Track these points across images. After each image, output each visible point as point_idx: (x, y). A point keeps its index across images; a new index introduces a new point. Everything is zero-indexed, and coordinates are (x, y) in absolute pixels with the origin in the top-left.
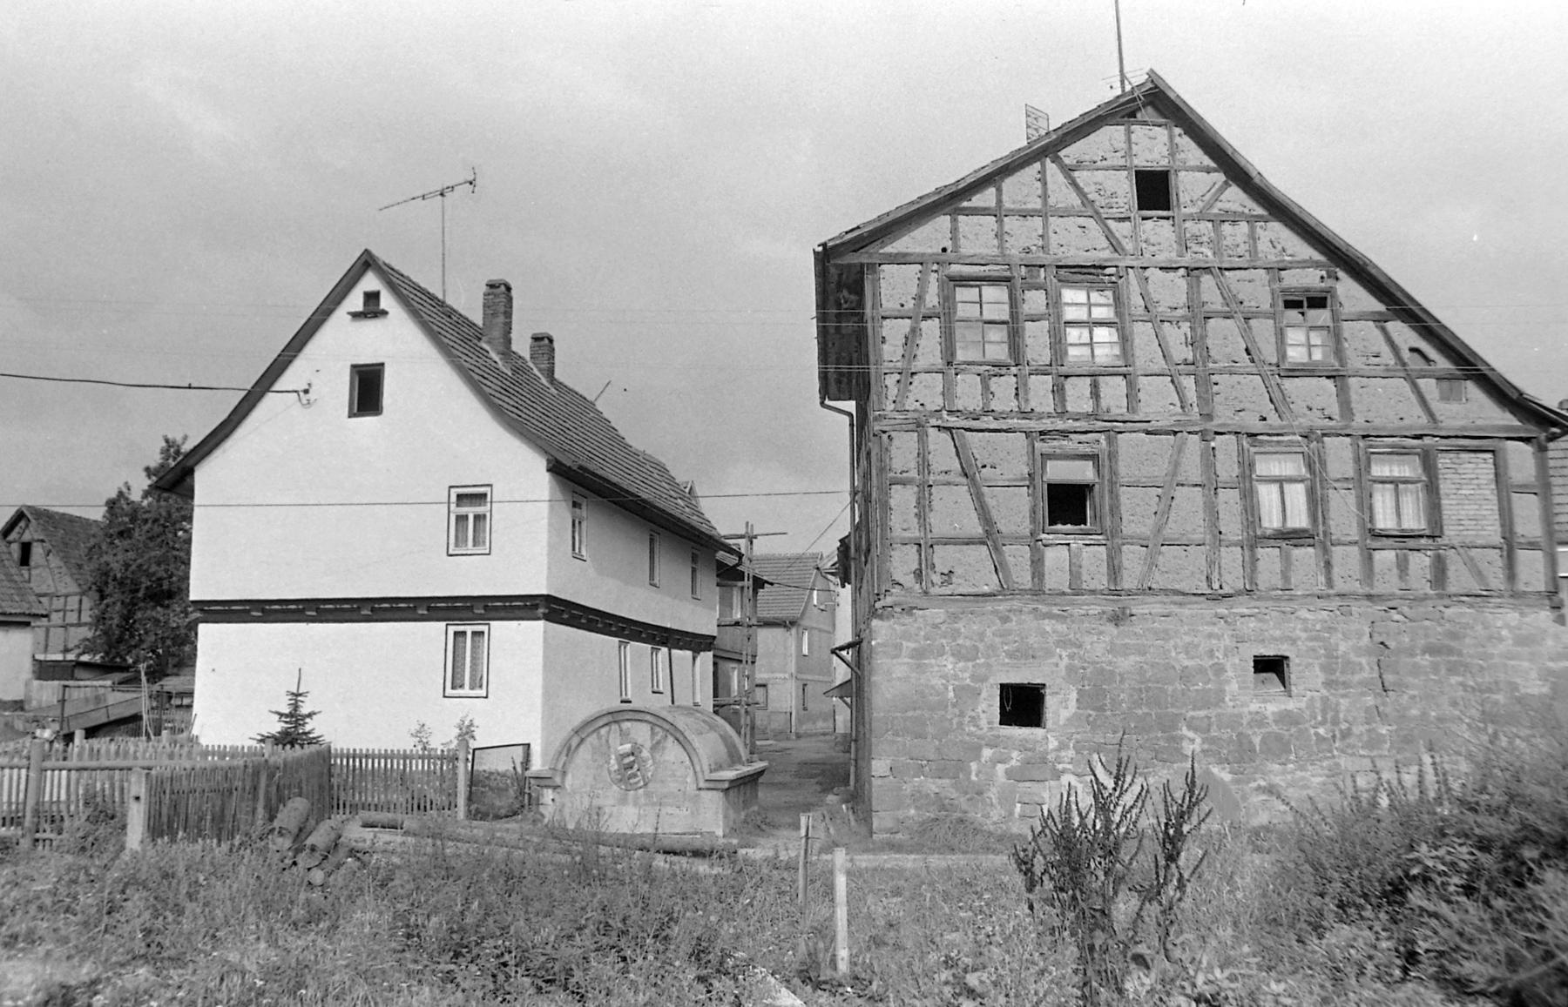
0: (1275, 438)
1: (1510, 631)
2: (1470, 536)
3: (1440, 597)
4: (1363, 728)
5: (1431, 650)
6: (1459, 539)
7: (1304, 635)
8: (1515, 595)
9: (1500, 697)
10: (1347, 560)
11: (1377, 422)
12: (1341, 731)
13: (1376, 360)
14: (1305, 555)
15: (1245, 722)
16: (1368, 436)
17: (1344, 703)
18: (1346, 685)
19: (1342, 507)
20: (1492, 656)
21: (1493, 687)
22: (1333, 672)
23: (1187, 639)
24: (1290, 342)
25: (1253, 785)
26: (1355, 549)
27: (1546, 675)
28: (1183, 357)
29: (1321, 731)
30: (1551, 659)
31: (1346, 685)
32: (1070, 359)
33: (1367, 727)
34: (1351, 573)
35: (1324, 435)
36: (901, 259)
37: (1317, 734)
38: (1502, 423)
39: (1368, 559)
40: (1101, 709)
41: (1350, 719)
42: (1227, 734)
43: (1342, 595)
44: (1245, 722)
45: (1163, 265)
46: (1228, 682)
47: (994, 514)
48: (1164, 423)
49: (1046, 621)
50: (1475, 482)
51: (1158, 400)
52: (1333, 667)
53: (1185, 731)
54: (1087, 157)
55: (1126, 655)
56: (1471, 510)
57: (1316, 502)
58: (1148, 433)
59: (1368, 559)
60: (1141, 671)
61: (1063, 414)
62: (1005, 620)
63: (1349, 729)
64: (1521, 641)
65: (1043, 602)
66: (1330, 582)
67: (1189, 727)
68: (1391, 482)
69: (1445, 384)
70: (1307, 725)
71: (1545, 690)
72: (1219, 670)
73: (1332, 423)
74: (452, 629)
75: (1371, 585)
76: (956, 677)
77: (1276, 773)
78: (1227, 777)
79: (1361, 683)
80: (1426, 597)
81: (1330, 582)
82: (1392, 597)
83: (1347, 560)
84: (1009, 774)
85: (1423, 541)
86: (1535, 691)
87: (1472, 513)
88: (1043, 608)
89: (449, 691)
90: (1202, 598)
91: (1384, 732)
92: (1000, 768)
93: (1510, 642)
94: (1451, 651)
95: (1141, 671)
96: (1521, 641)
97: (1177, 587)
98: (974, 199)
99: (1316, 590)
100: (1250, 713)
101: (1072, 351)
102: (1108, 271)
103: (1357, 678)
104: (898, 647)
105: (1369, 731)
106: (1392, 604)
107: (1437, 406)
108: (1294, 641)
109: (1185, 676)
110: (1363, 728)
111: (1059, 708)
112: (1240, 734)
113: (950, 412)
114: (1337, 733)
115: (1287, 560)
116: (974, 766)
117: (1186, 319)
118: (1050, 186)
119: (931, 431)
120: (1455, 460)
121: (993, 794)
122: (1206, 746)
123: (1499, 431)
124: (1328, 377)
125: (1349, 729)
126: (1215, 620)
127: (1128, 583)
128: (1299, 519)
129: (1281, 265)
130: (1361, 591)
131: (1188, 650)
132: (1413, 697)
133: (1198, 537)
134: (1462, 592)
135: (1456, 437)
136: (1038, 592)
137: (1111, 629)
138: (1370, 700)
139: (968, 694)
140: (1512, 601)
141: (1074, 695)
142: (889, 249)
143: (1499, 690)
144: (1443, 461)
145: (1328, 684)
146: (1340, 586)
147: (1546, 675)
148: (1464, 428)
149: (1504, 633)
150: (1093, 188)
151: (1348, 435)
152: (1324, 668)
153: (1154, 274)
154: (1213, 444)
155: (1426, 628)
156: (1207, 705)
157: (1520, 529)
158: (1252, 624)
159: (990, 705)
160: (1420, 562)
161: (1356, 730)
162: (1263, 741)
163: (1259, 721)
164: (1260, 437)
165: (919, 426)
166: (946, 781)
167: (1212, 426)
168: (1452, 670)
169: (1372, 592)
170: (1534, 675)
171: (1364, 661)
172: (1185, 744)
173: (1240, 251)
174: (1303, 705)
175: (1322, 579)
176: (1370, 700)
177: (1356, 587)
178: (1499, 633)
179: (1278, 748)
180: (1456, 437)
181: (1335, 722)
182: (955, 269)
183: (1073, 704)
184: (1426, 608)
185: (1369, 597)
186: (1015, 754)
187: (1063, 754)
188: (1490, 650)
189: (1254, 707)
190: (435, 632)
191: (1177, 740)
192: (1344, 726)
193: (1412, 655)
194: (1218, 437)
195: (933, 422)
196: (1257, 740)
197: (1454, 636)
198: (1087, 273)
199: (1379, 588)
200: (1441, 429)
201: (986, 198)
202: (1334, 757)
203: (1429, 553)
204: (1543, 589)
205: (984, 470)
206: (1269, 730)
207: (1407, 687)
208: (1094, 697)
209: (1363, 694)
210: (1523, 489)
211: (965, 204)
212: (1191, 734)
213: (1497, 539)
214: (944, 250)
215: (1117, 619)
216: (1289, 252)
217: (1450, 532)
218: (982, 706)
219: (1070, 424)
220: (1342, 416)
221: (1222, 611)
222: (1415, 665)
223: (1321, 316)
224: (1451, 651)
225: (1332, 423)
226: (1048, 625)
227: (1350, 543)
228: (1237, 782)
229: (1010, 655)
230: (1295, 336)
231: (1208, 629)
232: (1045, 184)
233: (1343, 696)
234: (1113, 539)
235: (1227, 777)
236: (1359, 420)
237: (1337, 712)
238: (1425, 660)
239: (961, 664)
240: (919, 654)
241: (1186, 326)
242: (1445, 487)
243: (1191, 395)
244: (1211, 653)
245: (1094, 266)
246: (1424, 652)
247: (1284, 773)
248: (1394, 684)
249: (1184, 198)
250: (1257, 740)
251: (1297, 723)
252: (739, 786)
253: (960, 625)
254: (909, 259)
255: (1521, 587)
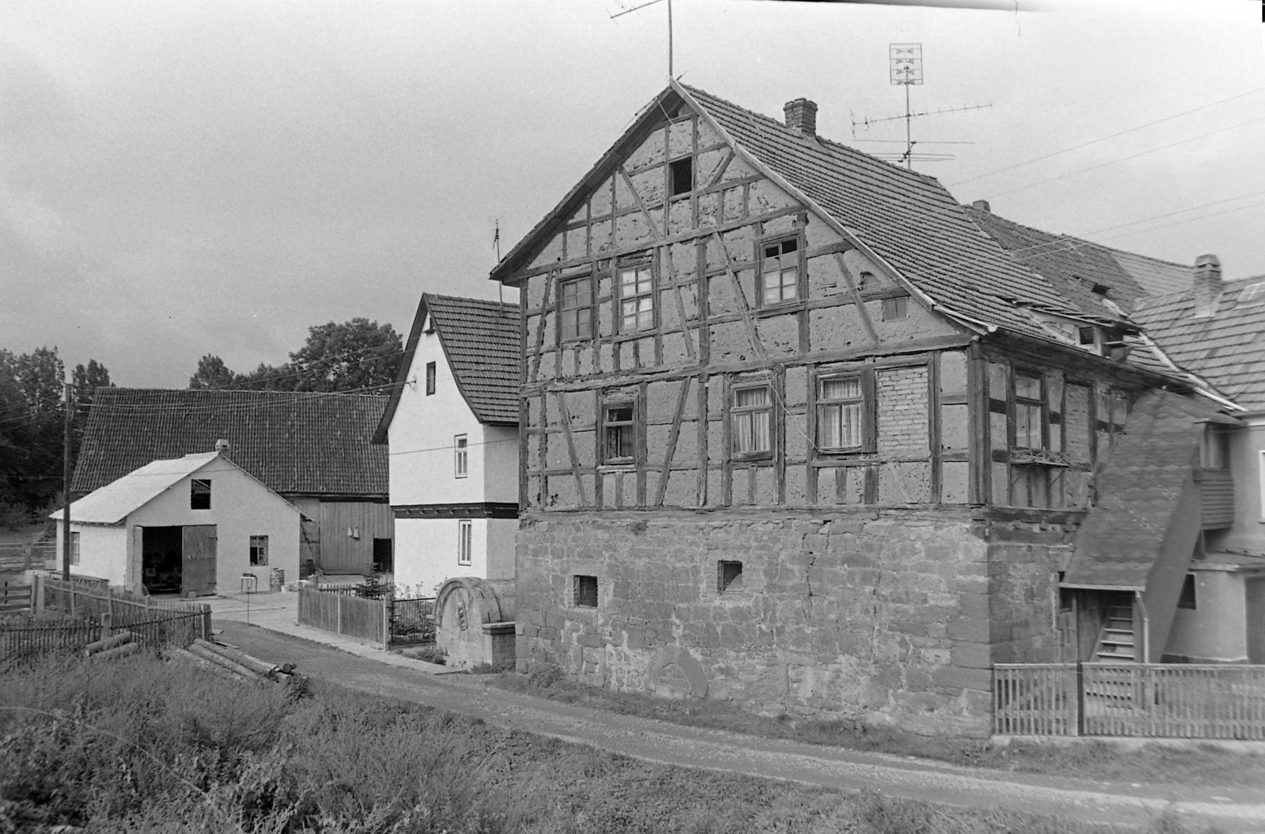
0: (751, 374)
1: (924, 544)
2: (903, 451)
3: (869, 510)
4: (794, 627)
5: (849, 560)
6: (892, 454)
7: (755, 544)
8: (940, 507)
9: (911, 609)
10: (797, 476)
11: (830, 349)
12: (777, 628)
13: (833, 291)
14: (766, 475)
15: (711, 614)
16: (820, 363)
17: (780, 605)
18: (782, 589)
19: (797, 428)
20: (905, 568)
21: (904, 597)
22: (773, 577)
23: (677, 546)
24: (768, 286)
25: (717, 666)
26: (804, 467)
27: (955, 588)
28: (692, 313)
29: (763, 627)
30: (961, 573)
31: (782, 589)
32: (625, 328)
33: (796, 626)
34: (799, 490)
35: (787, 367)
36: (537, 272)
37: (760, 629)
38: (938, 335)
39: (814, 473)
40: (626, 597)
41: (784, 619)
42: (701, 623)
43: (791, 510)
44: (711, 614)
45: (682, 239)
46: (701, 581)
47: (577, 455)
48: (676, 371)
49: (601, 531)
50: (909, 397)
51: (677, 353)
52: (774, 572)
53: (674, 619)
54: (640, 163)
55: (639, 557)
56: (904, 425)
57: (778, 429)
58: (669, 380)
59: (814, 473)
60: (649, 570)
61: (618, 372)
62: (578, 529)
63: (782, 627)
64: (933, 553)
65: (600, 516)
66: (782, 499)
67: (678, 617)
68: (837, 404)
69: (891, 304)
70: (754, 621)
71: (953, 603)
72: (696, 571)
73: (791, 355)
74: (462, 523)
75: (815, 501)
76: (553, 570)
77: (731, 658)
78: (699, 657)
79: (792, 587)
80: (857, 511)
81: (782, 499)
82: (830, 510)
83: (797, 476)
84: (579, 640)
85: (861, 458)
86: (944, 604)
87: (905, 428)
88: (600, 520)
89: (462, 562)
90: (694, 513)
91: (809, 632)
92: (575, 635)
93: (923, 554)
94: (866, 562)
95: (649, 570)
96: (933, 553)
97: (679, 504)
98: (576, 216)
99: (771, 506)
100: (715, 608)
101: (792, 281)
102: (649, 252)
103: (790, 583)
104: (526, 547)
105: (798, 630)
106: (827, 517)
107: (878, 326)
108: (747, 549)
109: (674, 574)
110: (794, 627)
111: (606, 593)
112: (708, 624)
113: (559, 380)
114: (774, 630)
115: (752, 478)
116: (562, 632)
117: (695, 282)
118: (617, 193)
119: (548, 394)
120: (893, 378)
121: (571, 653)
122: (687, 632)
123: (934, 344)
124: (792, 313)
125: (782, 627)
126: (696, 531)
127: (650, 501)
128: (765, 446)
129: (764, 218)
130: (805, 506)
131: (678, 554)
132: (831, 603)
133: (693, 463)
134: (889, 505)
135: (894, 355)
136: (598, 509)
137: (632, 536)
138: (798, 603)
139: (559, 581)
140: (936, 513)
141: (612, 587)
142: (532, 266)
143: (908, 601)
144: (884, 379)
145: (770, 587)
146: (790, 501)
147: (955, 588)
148: (900, 346)
149: (918, 545)
150: (642, 187)
151: (804, 365)
152: (766, 573)
153: (677, 248)
154: (706, 385)
155: (847, 540)
156: (688, 600)
157: (945, 442)
158: (721, 535)
159: (569, 591)
160: (856, 478)
161: (788, 629)
162: (723, 631)
163: (720, 615)
164: (742, 375)
165: (541, 393)
166: (549, 642)
167: (707, 370)
168: (865, 579)
169: (814, 506)
170: (943, 587)
171: (796, 568)
172: (674, 628)
173: (735, 213)
174: (751, 604)
175: (776, 496)
176: (798, 603)
177: (804, 503)
178: (913, 546)
179: (735, 638)
180: (894, 355)
181: (773, 620)
182: (567, 272)
183: (611, 592)
184: (856, 521)
185: (812, 511)
186: (581, 626)
187: (606, 629)
188: (905, 562)
189: (717, 603)
190: (453, 524)
191: (668, 624)
192: (779, 624)
193: (832, 565)
194: (712, 378)
195: (549, 389)
196: (719, 630)
197: (869, 547)
198: (634, 258)
199: (821, 504)
200: (880, 350)
201: (581, 215)
202: (772, 650)
203: (863, 469)
204: (966, 502)
205: (573, 421)
206: (727, 622)
207: (827, 594)
208: (623, 590)
209: (794, 598)
210: (953, 400)
211: (571, 222)
212: (678, 621)
213: (927, 453)
214: (559, 259)
215: (639, 529)
216: (771, 204)
217: (884, 446)
218: (566, 592)
219: (624, 379)
220: (801, 347)
221: (702, 524)
222: (836, 574)
223: (791, 258)
224: (866, 562)
225: (791, 355)
226: (600, 533)
227: (799, 463)
228: (706, 662)
229: (579, 555)
230: (772, 280)
231: (690, 538)
232: (614, 192)
233: (780, 598)
234: (641, 466)
235: (699, 657)
236: (815, 349)
237: (774, 612)
238: (843, 570)
239: (556, 561)
240: (536, 553)
241: (695, 287)
242: (883, 405)
243: (696, 345)
244: (692, 558)
245: (638, 251)
246: (843, 563)
247: (737, 658)
248: (819, 590)
249: (699, 178)
250: (719, 630)
251: (747, 619)
252: (505, 634)
253: (555, 533)
254: (542, 271)
255: (944, 500)
